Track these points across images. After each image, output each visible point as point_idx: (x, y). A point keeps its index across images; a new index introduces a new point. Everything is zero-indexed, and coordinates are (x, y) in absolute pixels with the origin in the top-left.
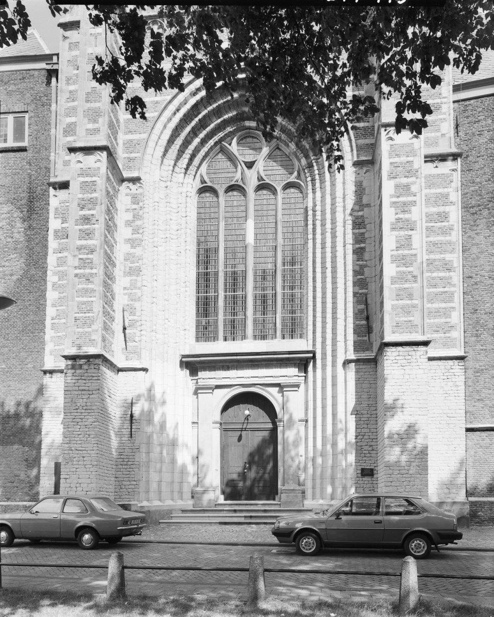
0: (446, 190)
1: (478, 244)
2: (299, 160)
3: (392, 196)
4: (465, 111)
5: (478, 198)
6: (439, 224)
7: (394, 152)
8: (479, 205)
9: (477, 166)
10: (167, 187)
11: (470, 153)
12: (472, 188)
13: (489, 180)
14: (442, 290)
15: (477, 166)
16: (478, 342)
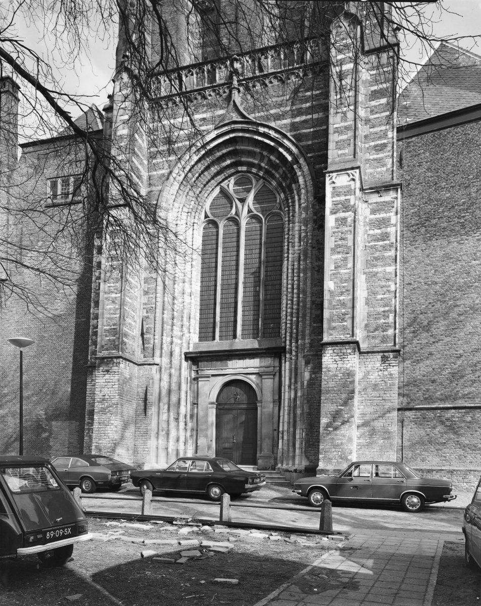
0: (388, 215)
1: (416, 256)
2: (279, 195)
3: (332, 228)
4: (408, 147)
5: (417, 219)
6: (381, 243)
7: (336, 193)
8: (418, 224)
9: (417, 192)
10: (177, 225)
11: (411, 182)
12: (413, 211)
13: (426, 203)
14: (382, 296)
15: (417, 192)
16: (415, 337)
